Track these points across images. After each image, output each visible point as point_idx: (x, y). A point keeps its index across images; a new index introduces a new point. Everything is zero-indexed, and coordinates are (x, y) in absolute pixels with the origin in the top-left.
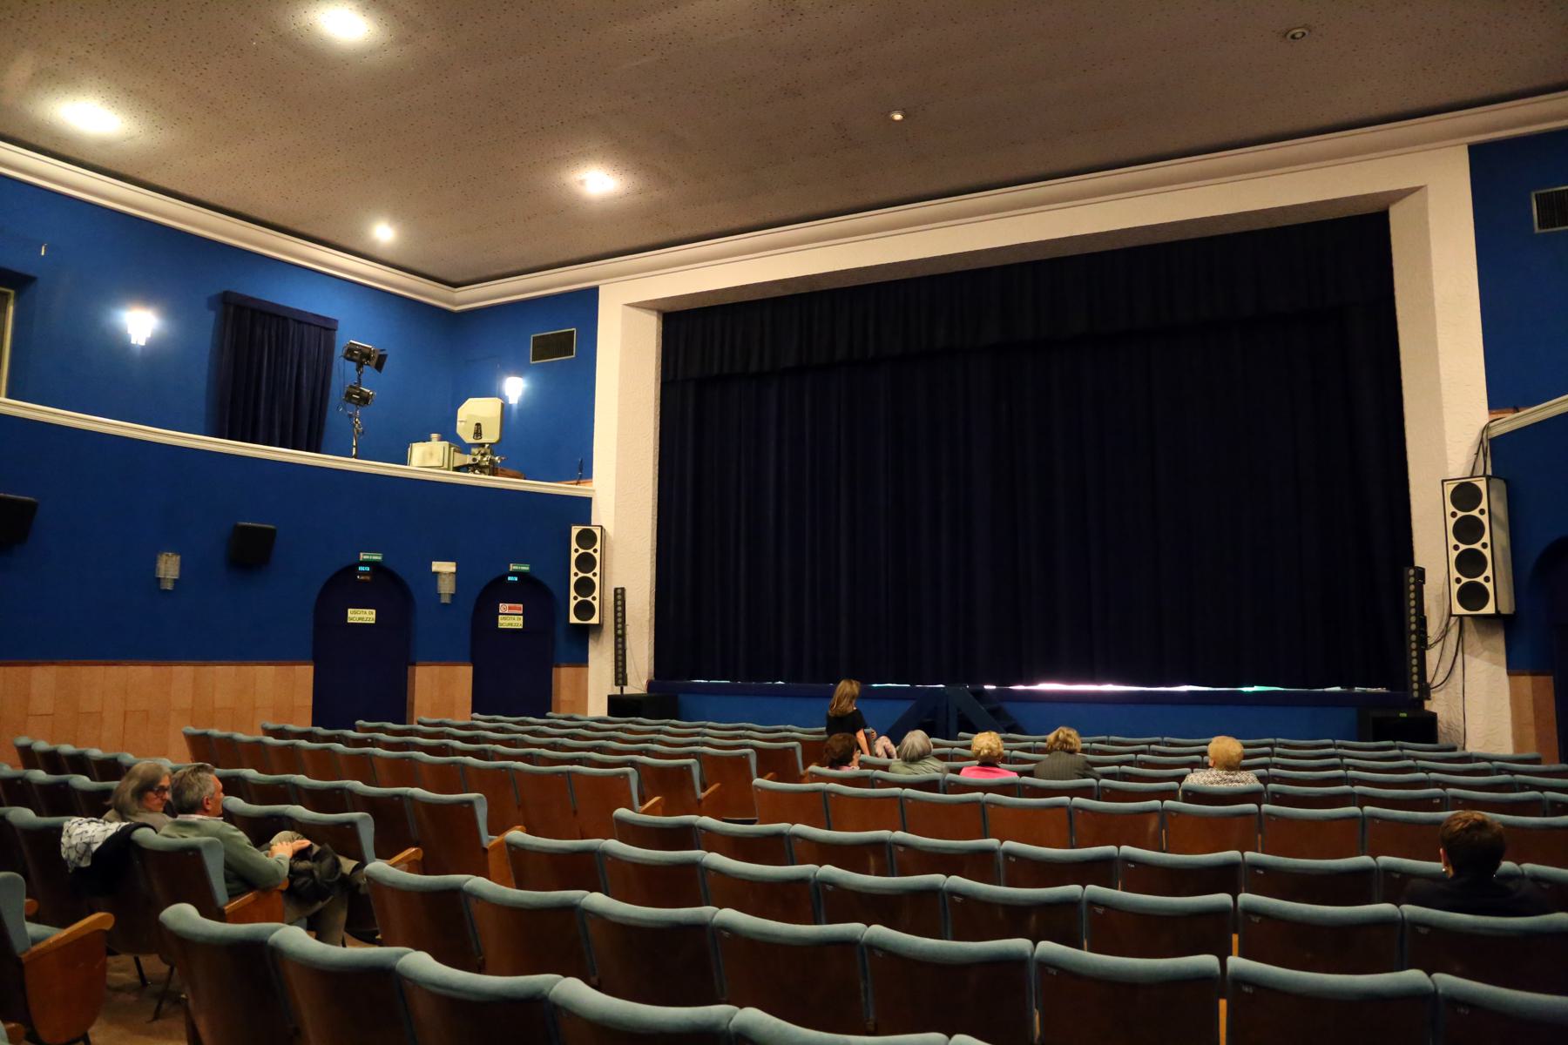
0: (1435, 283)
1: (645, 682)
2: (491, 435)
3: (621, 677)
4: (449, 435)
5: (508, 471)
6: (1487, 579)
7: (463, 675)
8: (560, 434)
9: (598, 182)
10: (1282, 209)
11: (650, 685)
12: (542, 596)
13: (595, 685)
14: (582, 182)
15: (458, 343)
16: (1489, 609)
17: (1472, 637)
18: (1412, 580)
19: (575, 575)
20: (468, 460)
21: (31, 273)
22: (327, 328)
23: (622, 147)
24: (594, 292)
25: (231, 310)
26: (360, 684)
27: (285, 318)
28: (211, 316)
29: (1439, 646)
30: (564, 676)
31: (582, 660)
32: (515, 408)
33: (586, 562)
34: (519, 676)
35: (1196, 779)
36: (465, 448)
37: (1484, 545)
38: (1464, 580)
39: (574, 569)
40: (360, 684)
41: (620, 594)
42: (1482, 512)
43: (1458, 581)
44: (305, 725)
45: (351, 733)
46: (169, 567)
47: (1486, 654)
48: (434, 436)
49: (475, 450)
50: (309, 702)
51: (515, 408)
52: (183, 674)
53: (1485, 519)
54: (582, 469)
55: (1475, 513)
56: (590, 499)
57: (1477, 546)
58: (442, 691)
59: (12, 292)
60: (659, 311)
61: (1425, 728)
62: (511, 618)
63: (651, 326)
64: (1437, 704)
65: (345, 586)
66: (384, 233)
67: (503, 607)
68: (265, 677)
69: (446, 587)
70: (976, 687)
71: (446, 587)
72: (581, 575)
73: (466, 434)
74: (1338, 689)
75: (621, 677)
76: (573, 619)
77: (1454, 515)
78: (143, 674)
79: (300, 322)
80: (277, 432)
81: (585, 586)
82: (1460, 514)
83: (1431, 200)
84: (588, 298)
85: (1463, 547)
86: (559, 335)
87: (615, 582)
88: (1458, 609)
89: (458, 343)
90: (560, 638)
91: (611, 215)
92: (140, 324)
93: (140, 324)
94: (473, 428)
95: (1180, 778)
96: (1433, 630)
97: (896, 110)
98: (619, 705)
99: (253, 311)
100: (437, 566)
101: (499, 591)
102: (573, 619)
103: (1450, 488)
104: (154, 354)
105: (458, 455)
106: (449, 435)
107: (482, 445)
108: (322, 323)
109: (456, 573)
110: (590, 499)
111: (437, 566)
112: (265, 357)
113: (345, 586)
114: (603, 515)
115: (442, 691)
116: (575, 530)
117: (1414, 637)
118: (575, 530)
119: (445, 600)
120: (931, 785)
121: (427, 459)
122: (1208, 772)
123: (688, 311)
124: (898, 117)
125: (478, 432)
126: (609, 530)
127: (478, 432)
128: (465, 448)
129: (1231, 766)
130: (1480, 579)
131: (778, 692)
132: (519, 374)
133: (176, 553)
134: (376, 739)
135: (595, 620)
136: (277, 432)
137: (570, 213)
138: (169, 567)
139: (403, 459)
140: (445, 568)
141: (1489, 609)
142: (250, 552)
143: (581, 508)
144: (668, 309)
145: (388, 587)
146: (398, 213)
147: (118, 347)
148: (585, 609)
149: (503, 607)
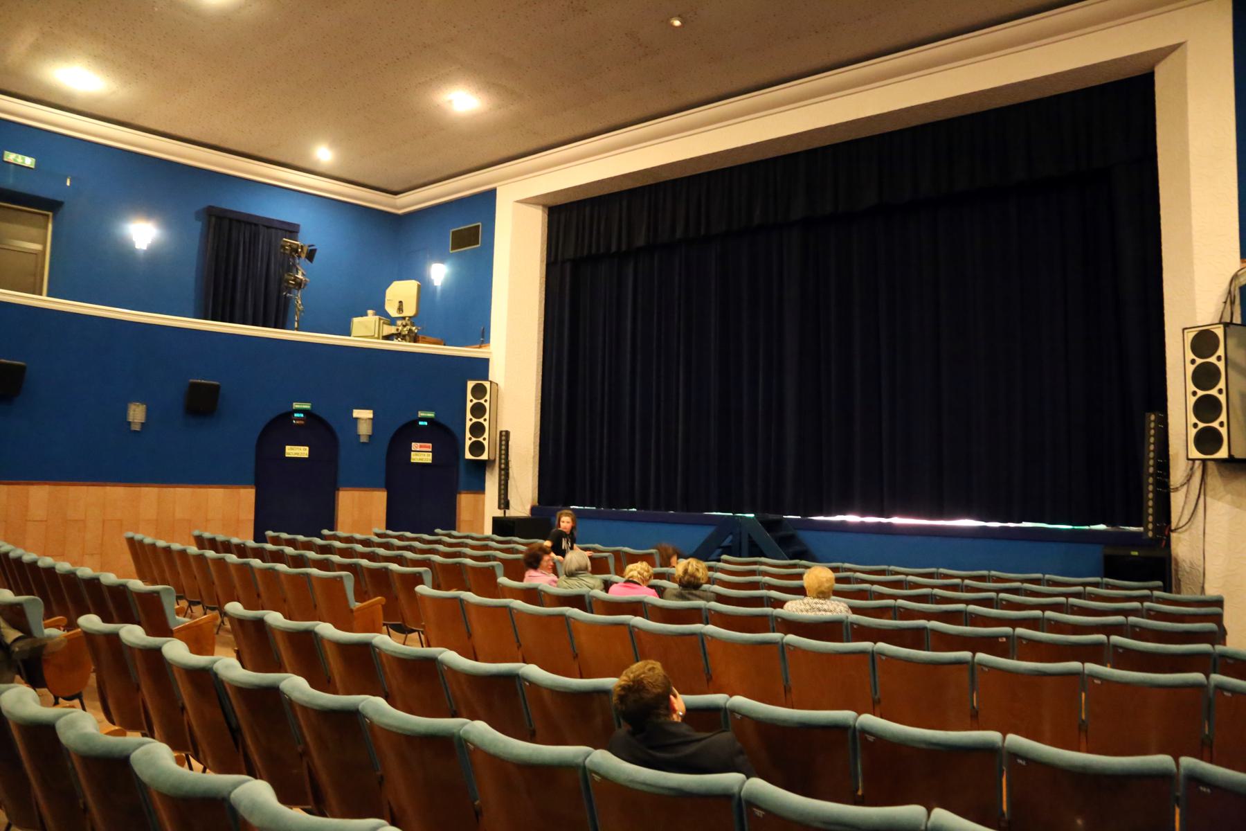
0: (1191, 136)
1: (528, 507)
2: (410, 310)
3: (504, 503)
4: (381, 311)
5: (428, 338)
6: (1221, 424)
7: (379, 499)
8: (468, 312)
9: (462, 101)
10: (1046, 78)
11: (533, 509)
12: (445, 437)
13: (482, 510)
14: (450, 102)
15: (393, 237)
16: (1223, 453)
17: (1214, 480)
18: (1152, 425)
19: (470, 420)
20: (393, 330)
21: (59, 199)
22: (292, 230)
23: (488, 68)
24: (492, 194)
25: (213, 219)
26: (292, 503)
27: (256, 225)
28: (198, 225)
29: (1184, 489)
30: (465, 501)
31: (480, 489)
32: (439, 289)
33: (479, 410)
34: (426, 500)
35: (796, 608)
36: (392, 321)
37: (1220, 391)
38: (1201, 425)
39: (469, 416)
40: (292, 503)
41: (505, 436)
42: (1219, 358)
43: (1195, 425)
44: (382, 530)
45: (318, 541)
46: (137, 414)
47: (1229, 497)
48: (370, 312)
49: (399, 322)
50: (252, 516)
51: (439, 289)
52: (149, 494)
53: (1221, 365)
54: (483, 337)
55: (1213, 360)
56: (487, 360)
57: (1214, 392)
58: (361, 511)
59: (50, 214)
60: (544, 206)
61: (1156, 565)
62: (421, 454)
63: (537, 220)
64: (1182, 547)
65: (281, 428)
66: (324, 154)
67: (415, 446)
68: (216, 497)
69: (364, 430)
70: (772, 517)
71: (364, 430)
72: (475, 420)
73: (392, 311)
74: (1102, 527)
75: (504, 503)
76: (468, 456)
77: (1193, 362)
78: (117, 494)
79: (268, 227)
80: (250, 312)
81: (478, 429)
82: (1199, 361)
83: (1190, 54)
84: (487, 200)
85: (1200, 393)
86: (468, 227)
87: (503, 427)
88: (1195, 454)
89: (393, 237)
90: (459, 471)
91: (475, 131)
92: (142, 234)
93: (142, 234)
94: (397, 305)
95: (780, 604)
96: (1178, 473)
97: (680, 17)
98: (503, 526)
99: (231, 220)
100: (357, 413)
101: (410, 432)
102: (468, 456)
103: (1190, 336)
104: (153, 256)
105: (386, 327)
106: (381, 311)
107: (404, 318)
108: (286, 227)
109: (372, 419)
110: (487, 360)
111: (357, 413)
112: (241, 256)
113: (281, 428)
114: (496, 372)
115: (361, 511)
116: (471, 384)
117: (1151, 480)
118: (471, 384)
119: (363, 439)
120: (578, 601)
121: (365, 332)
122: (807, 600)
123: (566, 205)
124: (677, 23)
125: (400, 309)
126: (502, 385)
127: (400, 309)
128: (392, 321)
129: (823, 595)
130: (1215, 424)
131: (631, 518)
132: (442, 261)
133: (142, 402)
134: (438, 547)
135: (485, 457)
136: (250, 312)
137: (438, 129)
138: (137, 414)
139: (347, 332)
140: (363, 415)
141: (1223, 453)
142: (202, 403)
143: (480, 368)
144: (552, 202)
145: (318, 429)
146: (335, 143)
147: (125, 253)
148: (477, 448)
149: (415, 446)
